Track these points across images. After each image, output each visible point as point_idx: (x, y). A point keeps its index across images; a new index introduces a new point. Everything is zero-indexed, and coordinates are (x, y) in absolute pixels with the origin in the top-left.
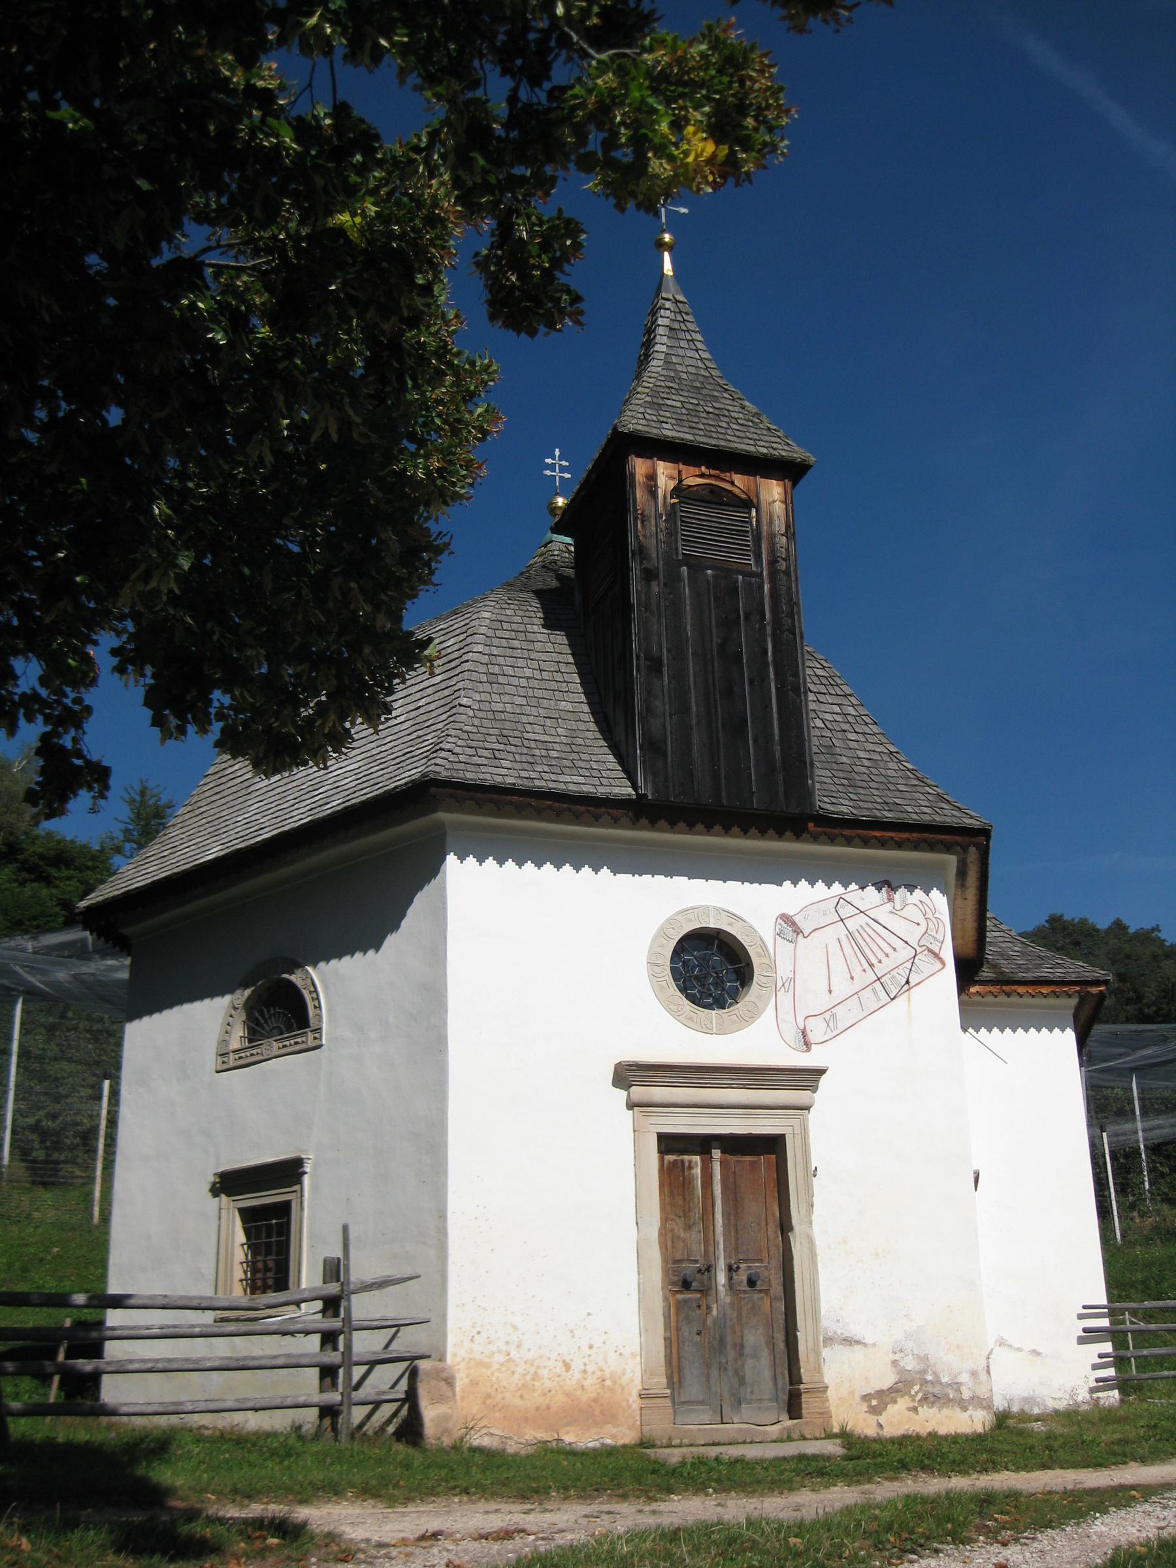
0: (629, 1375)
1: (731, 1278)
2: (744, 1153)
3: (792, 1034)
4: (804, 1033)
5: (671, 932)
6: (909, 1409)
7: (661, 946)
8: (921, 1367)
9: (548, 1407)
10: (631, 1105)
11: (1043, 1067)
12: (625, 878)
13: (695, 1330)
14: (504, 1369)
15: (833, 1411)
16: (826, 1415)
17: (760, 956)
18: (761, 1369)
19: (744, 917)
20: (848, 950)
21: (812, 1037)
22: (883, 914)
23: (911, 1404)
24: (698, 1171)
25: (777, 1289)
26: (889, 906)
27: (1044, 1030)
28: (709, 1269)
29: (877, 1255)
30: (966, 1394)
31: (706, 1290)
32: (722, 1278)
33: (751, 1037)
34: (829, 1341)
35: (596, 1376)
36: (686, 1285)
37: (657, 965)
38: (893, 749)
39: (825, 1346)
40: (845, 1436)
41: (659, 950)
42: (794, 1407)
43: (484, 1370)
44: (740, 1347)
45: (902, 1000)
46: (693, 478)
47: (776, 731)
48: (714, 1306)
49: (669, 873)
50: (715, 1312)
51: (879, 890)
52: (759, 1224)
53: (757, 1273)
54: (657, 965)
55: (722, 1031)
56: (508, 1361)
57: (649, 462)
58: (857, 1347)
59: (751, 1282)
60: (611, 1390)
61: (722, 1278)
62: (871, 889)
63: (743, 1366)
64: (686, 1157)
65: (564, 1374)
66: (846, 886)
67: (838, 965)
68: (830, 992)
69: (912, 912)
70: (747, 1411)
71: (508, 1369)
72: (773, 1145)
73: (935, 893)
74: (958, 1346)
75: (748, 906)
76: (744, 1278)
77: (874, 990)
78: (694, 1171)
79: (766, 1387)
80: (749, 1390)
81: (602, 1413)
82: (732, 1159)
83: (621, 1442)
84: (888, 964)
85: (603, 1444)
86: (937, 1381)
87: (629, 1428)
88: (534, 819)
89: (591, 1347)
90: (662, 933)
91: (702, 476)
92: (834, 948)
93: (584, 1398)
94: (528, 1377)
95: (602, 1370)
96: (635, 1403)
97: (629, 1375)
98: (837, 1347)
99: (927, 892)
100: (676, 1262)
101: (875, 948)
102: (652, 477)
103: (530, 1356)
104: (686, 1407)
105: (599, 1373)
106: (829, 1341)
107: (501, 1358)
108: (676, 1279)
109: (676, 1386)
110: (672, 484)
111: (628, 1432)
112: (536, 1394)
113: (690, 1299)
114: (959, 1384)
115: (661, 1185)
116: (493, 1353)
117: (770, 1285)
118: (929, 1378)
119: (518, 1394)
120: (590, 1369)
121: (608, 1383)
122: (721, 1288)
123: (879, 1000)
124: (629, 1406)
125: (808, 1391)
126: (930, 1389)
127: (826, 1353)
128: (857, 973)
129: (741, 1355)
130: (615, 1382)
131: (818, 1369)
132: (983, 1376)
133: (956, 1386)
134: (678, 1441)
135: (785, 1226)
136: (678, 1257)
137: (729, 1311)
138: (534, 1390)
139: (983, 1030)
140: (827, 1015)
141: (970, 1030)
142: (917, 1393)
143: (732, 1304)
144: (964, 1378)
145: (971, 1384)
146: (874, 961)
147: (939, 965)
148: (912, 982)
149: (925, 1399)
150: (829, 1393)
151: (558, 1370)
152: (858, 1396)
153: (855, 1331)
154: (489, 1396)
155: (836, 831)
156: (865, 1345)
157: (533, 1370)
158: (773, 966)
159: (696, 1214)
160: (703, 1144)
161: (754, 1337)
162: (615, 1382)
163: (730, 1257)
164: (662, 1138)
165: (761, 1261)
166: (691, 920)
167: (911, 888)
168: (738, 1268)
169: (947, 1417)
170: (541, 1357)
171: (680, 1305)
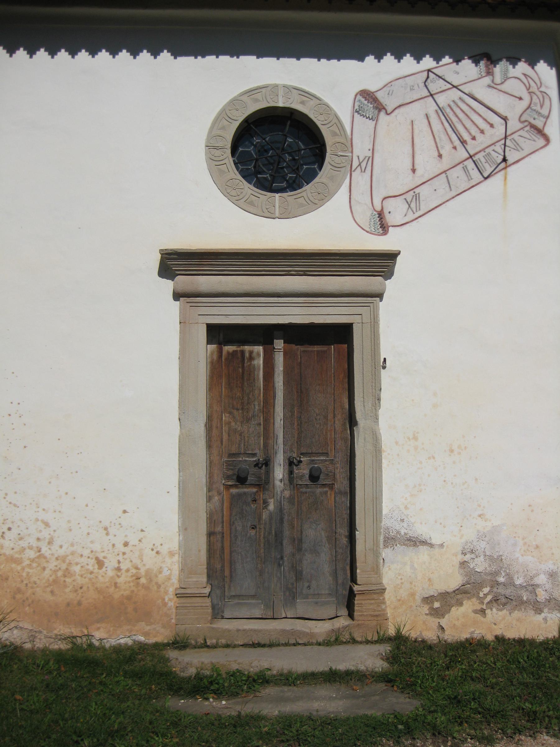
0: (166, 572)
1: (291, 472)
2: (312, 342)
3: (365, 215)
4: (381, 215)
6: (476, 612)
7: (223, 128)
8: (494, 568)
9: (79, 603)
10: (177, 296)
12: (187, 62)
13: (249, 524)
14: (34, 565)
15: (389, 613)
16: (381, 617)
17: (334, 134)
18: (321, 564)
20: (437, 126)
21: (390, 219)
22: (481, 89)
23: (479, 607)
25: (342, 484)
26: (487, 80)
28: (266, 464)
29: (452, 451)
30: (542, 596)
31: (264, 483)
32: (279, 472)
33: (325, 222)
34: (391, 540)
35: (130, 574)
36: (241, 480)
37: (215, 148)
39: (386, 546)
40: (399, 640)
41: (220, 132)
43: (14, 565)
44: (298, 543)
45: (498, 179)
48: (271, 501)
49: (235, 52)
50: (271, 507)
51: (476, 62)
52: (326, 417)
53: (319, 469)
54: (215, 148)
55: (286, 215)
56: (39, 557)
58: (423, 549)
59: (314, 478)
60: (146, 588)
61: (279, 472)
62: (467, 63)
63: (301, 561)
64: (247, 348)
65: (96, 570)
66: (438, 59)
67: (424, 141)
68: (414, 171)
69: (512, 86)
70: (301, 608)
71: (39, 564)
72: (342, 334)
74: (537, 547)
76: (306, 472)
77: (465, 169)
78: (255, 362)
79: (325, 581)
80: (306, 584)
81: (135, 610)
82: (299, 349)
83: (152, 640)
84: (482, 141)
85: (134, 641)
86: (510, 583)
87: (164, 627)
89: (126, 544)
92: (421, 126)
93: (116, 596)
94: (60, 574)
95: (137, 568)
96: (172, 602)
97: (166, 572)
98: (399, 548)
99: (532, 64)
100: (231, 455)
101: (468, 124)
103: (61, 552)
104: (236, 601)
105: (134, 571)
106: (391, 540)
107: (32, 554)
108: (230, 473)
109: (227, 580)
111: (162, 630)
112: (67, 590)
113: (245, 493)
114: (535, 586)
116: (23, 549)
117: (334, 479)
118: (501, 579)
119: (49, 589)
120: (124, 567)
121: (143, 580)
122: (277, 483)
123: (470, 178)
124: (165, 604)
125: (362, 593)
126: (501, 590)
127: (386, 553)
128: (446, 149)
129: (300, 550)
130: (150, 580)
131: (376, 570)
133: (532, 588)
134: (214, 641)
135: (352, 420)
136: (234, 450)
137: (286, 506)
138: (66, 586)
140: (409, 196)
142: (486, 595)
143: (291, 500)
144: (542, 579)
145: (548, 586)
146: (466, 137)
147: (542, 142)
148: (512, 156)
149: (496, 600)
150: (387, 595)
151: (90, 568)
152: (418, 598)
153: (421, 530)
154: (19, 590)
156: (431, 545)
157: (64, 566)
159: (257, 406)
160: (265, 334)
161: (315, 532)
162: (150, 580)
163: (292, 451)
165: (326, 454)
166: (256, 100)
167: (514, 61)
168: (300, 462)
169: (518, 620)
170: (73, 553)
171: (234, 499)
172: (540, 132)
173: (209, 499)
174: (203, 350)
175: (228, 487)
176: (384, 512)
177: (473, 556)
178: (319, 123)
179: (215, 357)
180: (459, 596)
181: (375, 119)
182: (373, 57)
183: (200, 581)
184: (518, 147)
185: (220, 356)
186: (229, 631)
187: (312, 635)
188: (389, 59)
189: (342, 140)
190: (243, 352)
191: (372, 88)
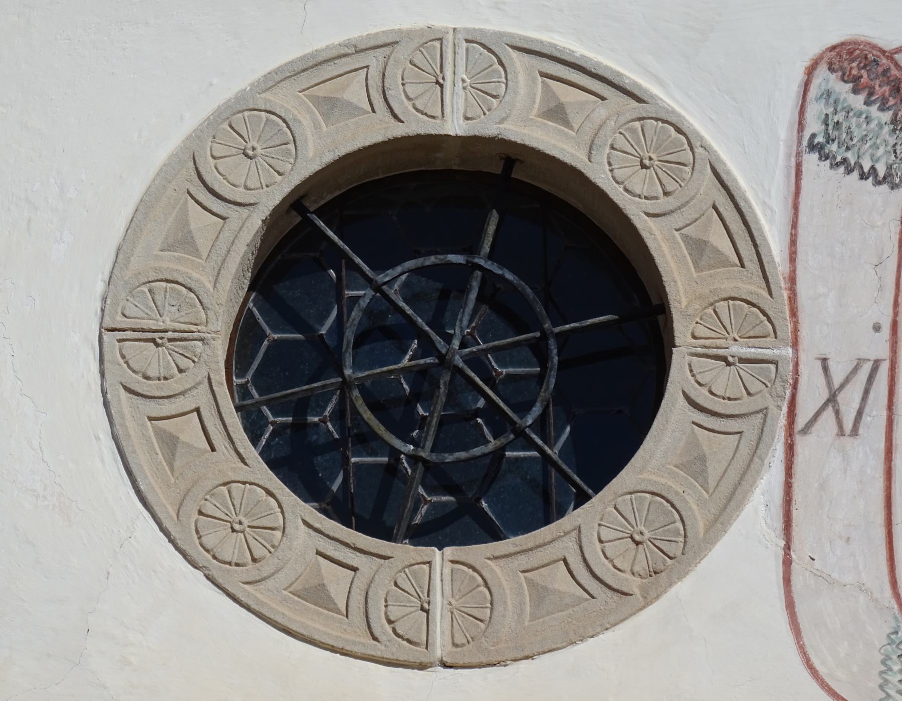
19: (632, 76)
37: (153, 337)
54: (153, 337)
90: (195, 178)
158: (771, 303)
189: (752, 287)
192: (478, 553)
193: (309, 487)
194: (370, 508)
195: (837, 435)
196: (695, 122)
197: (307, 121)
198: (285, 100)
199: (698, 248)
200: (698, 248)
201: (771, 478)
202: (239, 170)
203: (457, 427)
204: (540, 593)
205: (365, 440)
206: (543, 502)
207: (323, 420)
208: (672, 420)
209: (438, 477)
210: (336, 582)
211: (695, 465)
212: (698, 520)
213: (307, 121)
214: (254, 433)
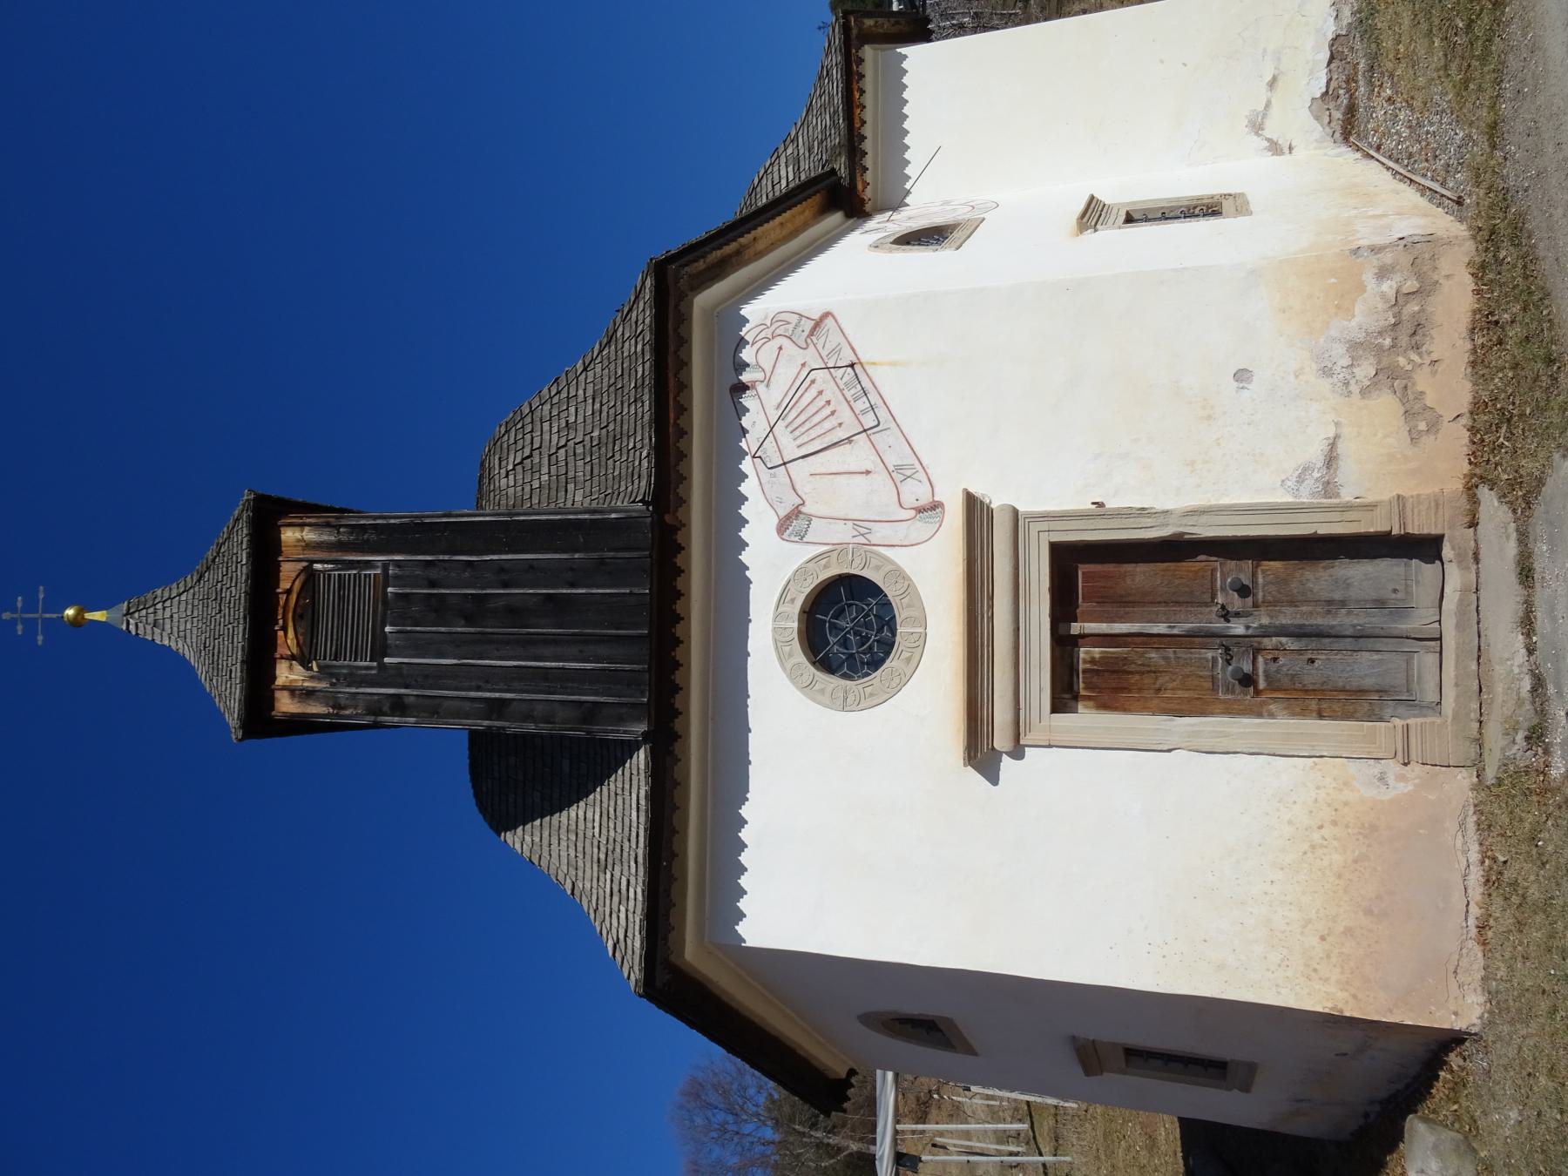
3: (920, 528)
4: (920, 510)
5: (807, 679)
6: (1434, 373)
11: (946, 90)
16: (1437, 503)
19: (784, 582)
21: (925, 500)
23: (1427, 369)
24: (1097, 652)
26: (761, 388)
27: (905, 80)
29: (1209, 417)
34: (1329, 488)
37: (845, 699)
38: (580, 367)
39: (1337, 495)
42: (1426, 548)
46: (288, 641)
47: (557, 556)
53: (1233, 582)
54: (845, 699)
57: (278, 694)
58: (1341, 448)
64: (1081, 666)
68: (868, 472)
69: (766, 359)
72: (1066, 558)
73: (746, 311)
75: (776, 572)
88: (685, 855)
90: (807, 688)
91: (284, 629)
98: (1340, 478)
101: (812, 409)
102: (292, 691)
106: (1329, 488)
110: (298, 667)
113: (1265, 671)
115: (1124, 709)
118: (1388, 342)
127: (1347, 496)
132: (1388, 258)
139: (908, 171)
141: (908, 186)
144: (1388, 287)
145: (1398, 277)
147: (829, 321)
148: (848, 357)
153: (1315, 452)
155: (672, 452)
156: (1337, 437)
158: (839, 549)
160: (1063, 645)
164: (1055, 709)
172: (818, 324)
173: (1272, 715)
174: (1085, 719)
175: (1257, 692)
176: (1290, 499)
177: (1353, 382)
178: (816, 582)
179: (1091, 703)
180: (1411, 397)
181: (809, 518)
182: (741, 928)
183: (1384, 732)
184: (836, 350)
185: (1088, 698)
186: (1457, 697)
187: (1464, 590)
188: (745, 511)
189: (835, 555)
190: (1084, 671)
191: (776, 521)
192: (898, 621)
193: (883, 661)
194: (888, 646)
195: (1074, 1038)
196: (795, 567)
197: (794, 660)
198: (788, 666)
199: (826, 567)
200: (826, 567)
201: (882, 550)
202: (805, 677)
203: (868, 625)
204: (909, 606)
205: (871, 648)
206: (887, 605)
207: (866, 658)
208: (866, 573)
209: (880, 630)
210: (905, 655)
211: (878, 568)
212: (890, 567)
213: (794, 660)
214: (868, 675)
